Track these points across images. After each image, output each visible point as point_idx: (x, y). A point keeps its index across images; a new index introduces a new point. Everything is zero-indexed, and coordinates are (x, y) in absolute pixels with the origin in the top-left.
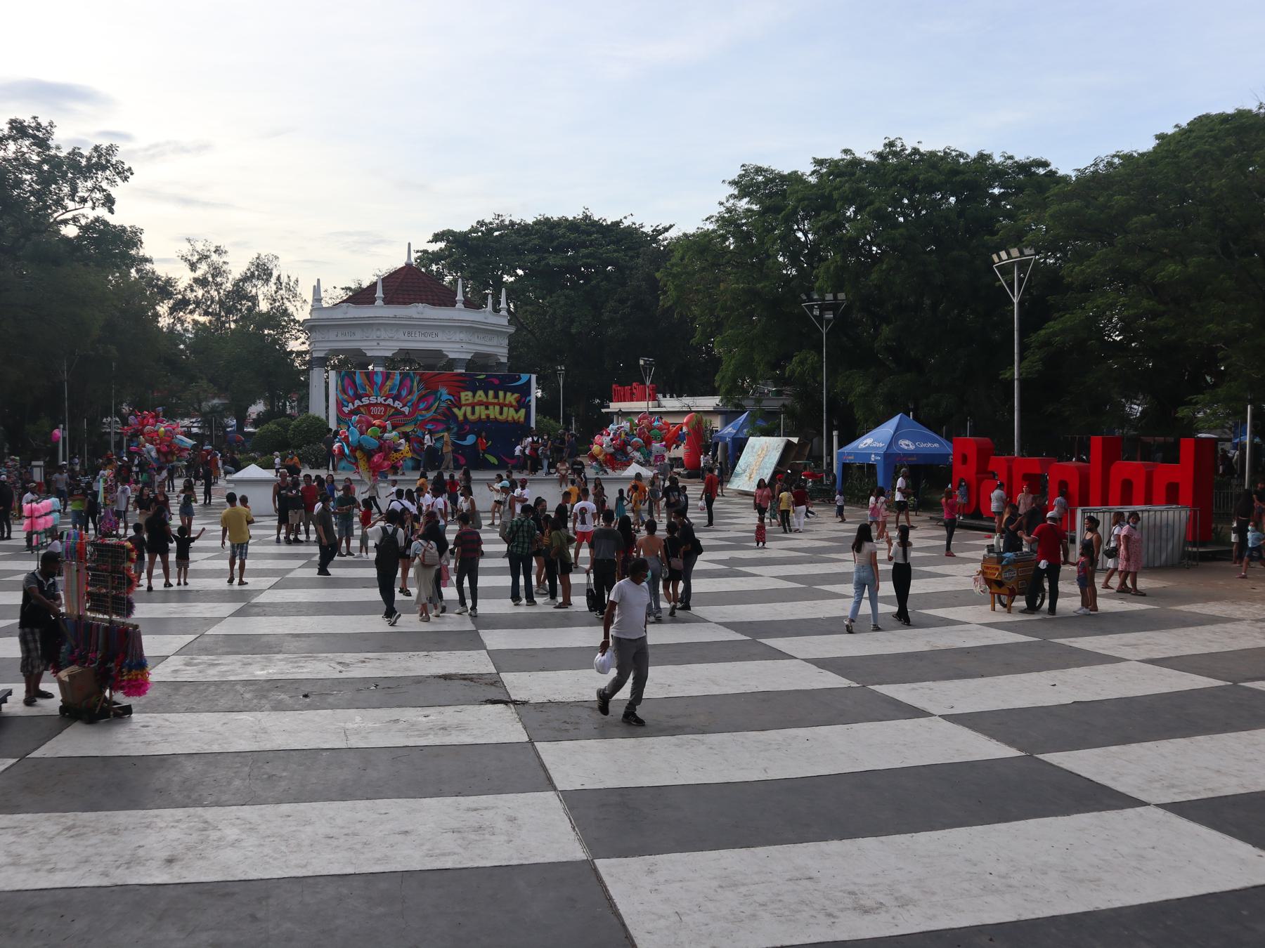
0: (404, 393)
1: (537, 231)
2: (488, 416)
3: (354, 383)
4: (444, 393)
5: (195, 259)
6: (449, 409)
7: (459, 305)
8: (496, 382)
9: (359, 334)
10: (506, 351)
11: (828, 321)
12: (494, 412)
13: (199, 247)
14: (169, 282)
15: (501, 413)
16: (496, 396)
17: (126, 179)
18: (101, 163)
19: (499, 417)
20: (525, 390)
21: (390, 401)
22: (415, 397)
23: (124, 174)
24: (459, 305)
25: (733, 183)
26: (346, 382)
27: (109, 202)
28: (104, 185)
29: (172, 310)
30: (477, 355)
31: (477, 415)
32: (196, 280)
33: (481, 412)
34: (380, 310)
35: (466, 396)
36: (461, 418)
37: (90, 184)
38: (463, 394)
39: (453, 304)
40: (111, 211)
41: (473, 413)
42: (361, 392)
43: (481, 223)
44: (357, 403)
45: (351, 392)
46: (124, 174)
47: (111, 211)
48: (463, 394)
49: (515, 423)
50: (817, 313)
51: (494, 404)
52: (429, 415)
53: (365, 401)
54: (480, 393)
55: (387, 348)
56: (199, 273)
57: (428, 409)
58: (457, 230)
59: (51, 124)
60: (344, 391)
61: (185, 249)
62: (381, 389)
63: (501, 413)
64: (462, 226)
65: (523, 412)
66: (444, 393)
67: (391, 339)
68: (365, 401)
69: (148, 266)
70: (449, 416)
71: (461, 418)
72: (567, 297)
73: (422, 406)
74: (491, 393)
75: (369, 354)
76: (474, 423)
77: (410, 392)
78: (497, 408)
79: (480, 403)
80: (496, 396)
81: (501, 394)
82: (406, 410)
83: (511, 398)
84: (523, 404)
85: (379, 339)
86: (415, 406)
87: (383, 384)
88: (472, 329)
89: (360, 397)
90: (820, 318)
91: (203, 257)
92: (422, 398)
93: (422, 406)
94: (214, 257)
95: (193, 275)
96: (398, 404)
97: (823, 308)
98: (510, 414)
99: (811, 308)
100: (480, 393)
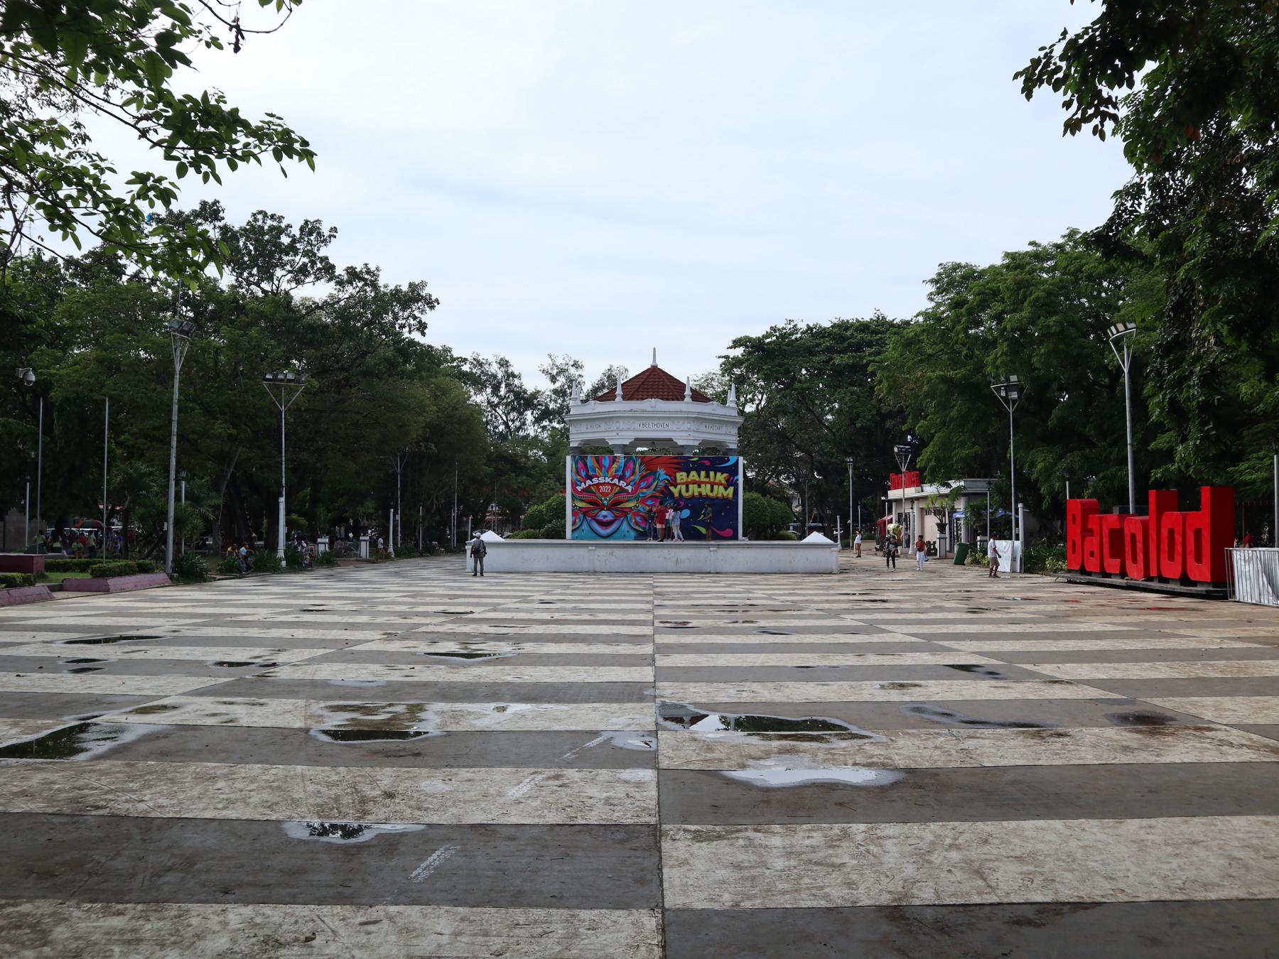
0: (628, 474)
1: (830, 334)
2: (700, 494)
3: (586, 465)
4: (662, 473)
5: (555, 372)
6: (666, 487)
7: (688, 399)
8: (708, 463)
9: (603, 426)
10: (736, 439)
11: (1014, 401)
12: (705, 490)
13: (559, 361)
14: (536, 394)
15: (712, 490)
16: (708, 476)
17: (432, 308)
18: (413, 297)
19: (710, 494)
20: (733, 470)
21: (616, 481)
22: (637, 477)
23: (431, 303)
24: (688, 399)
25: (932, 281)
26: (580, 465)
27: (422, 327)
28: (417, 313)
29: (538, 420)
30: (704, 442)
31: (690, 493)
32: (555, 392)
33: (694, 490)
34: (619, 405)
35: (681, 476)
36: (676, 495)
37: (406, 314)
38: (678, 475)
39: (683, 398)
40: (423, 334)
41: (687, 490)
42: (591, 473)
43: (774, 329)
44: (589, 482)
45: (583, 474)
46: (431, 303)
47: (423, 334)
48: (678, 475)
49: (725, 499)
50: (1003, 394)
51: (705, 483)
52: (649, 492)
53: (595, 481)
54: (693, 473)
55: (625, 438)
56: (558, 385)
57: (648, 487)
58: (753, 335)
59: (378, 269)
60: (578, 473)
61: (547, 363)
62: (608, 471)
63: (712, 490)
64: (756, 332)
65: (731, 489)
66: (662, 473)
67: (628, 430)
68: (595, 481)
69: (517, 382)
70: (666, 493)
71: (676, 495)
72: (853, 393)
73: (643, 485)
74: (703, 473)
75: (611, 443)
76: (688, 499)
77: (633, 473)
78: (709, 486)
79: (694, 482)
80: (708, 476)
81: (712, 474)
82: (630, 488)
83: (721, 477)
84: (731, 482)
85: (619, 430)
86: (637, 486)
87: (610, 466)
88: (699, 419)
89: (590, 478)
90: (1006, 399)
91: (562, 371)
92: (643, 478)
93: (643, 485)
94: (572, 370)
95: (553, 387)
96: (623, 484)
97: (1008, 389)
98: (720, 491)
99: (998, 389)
100: (693, 473)
